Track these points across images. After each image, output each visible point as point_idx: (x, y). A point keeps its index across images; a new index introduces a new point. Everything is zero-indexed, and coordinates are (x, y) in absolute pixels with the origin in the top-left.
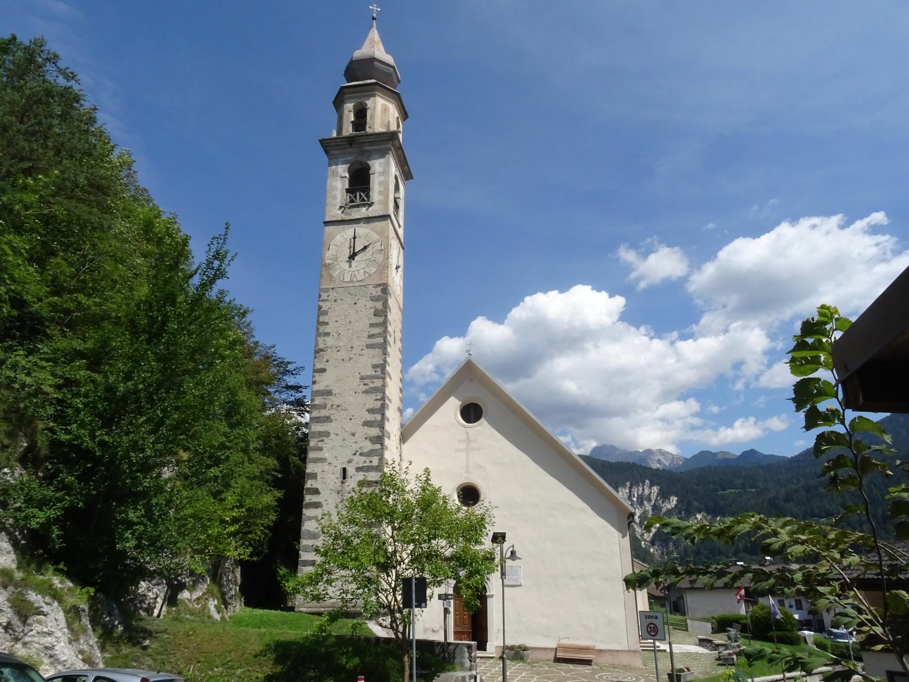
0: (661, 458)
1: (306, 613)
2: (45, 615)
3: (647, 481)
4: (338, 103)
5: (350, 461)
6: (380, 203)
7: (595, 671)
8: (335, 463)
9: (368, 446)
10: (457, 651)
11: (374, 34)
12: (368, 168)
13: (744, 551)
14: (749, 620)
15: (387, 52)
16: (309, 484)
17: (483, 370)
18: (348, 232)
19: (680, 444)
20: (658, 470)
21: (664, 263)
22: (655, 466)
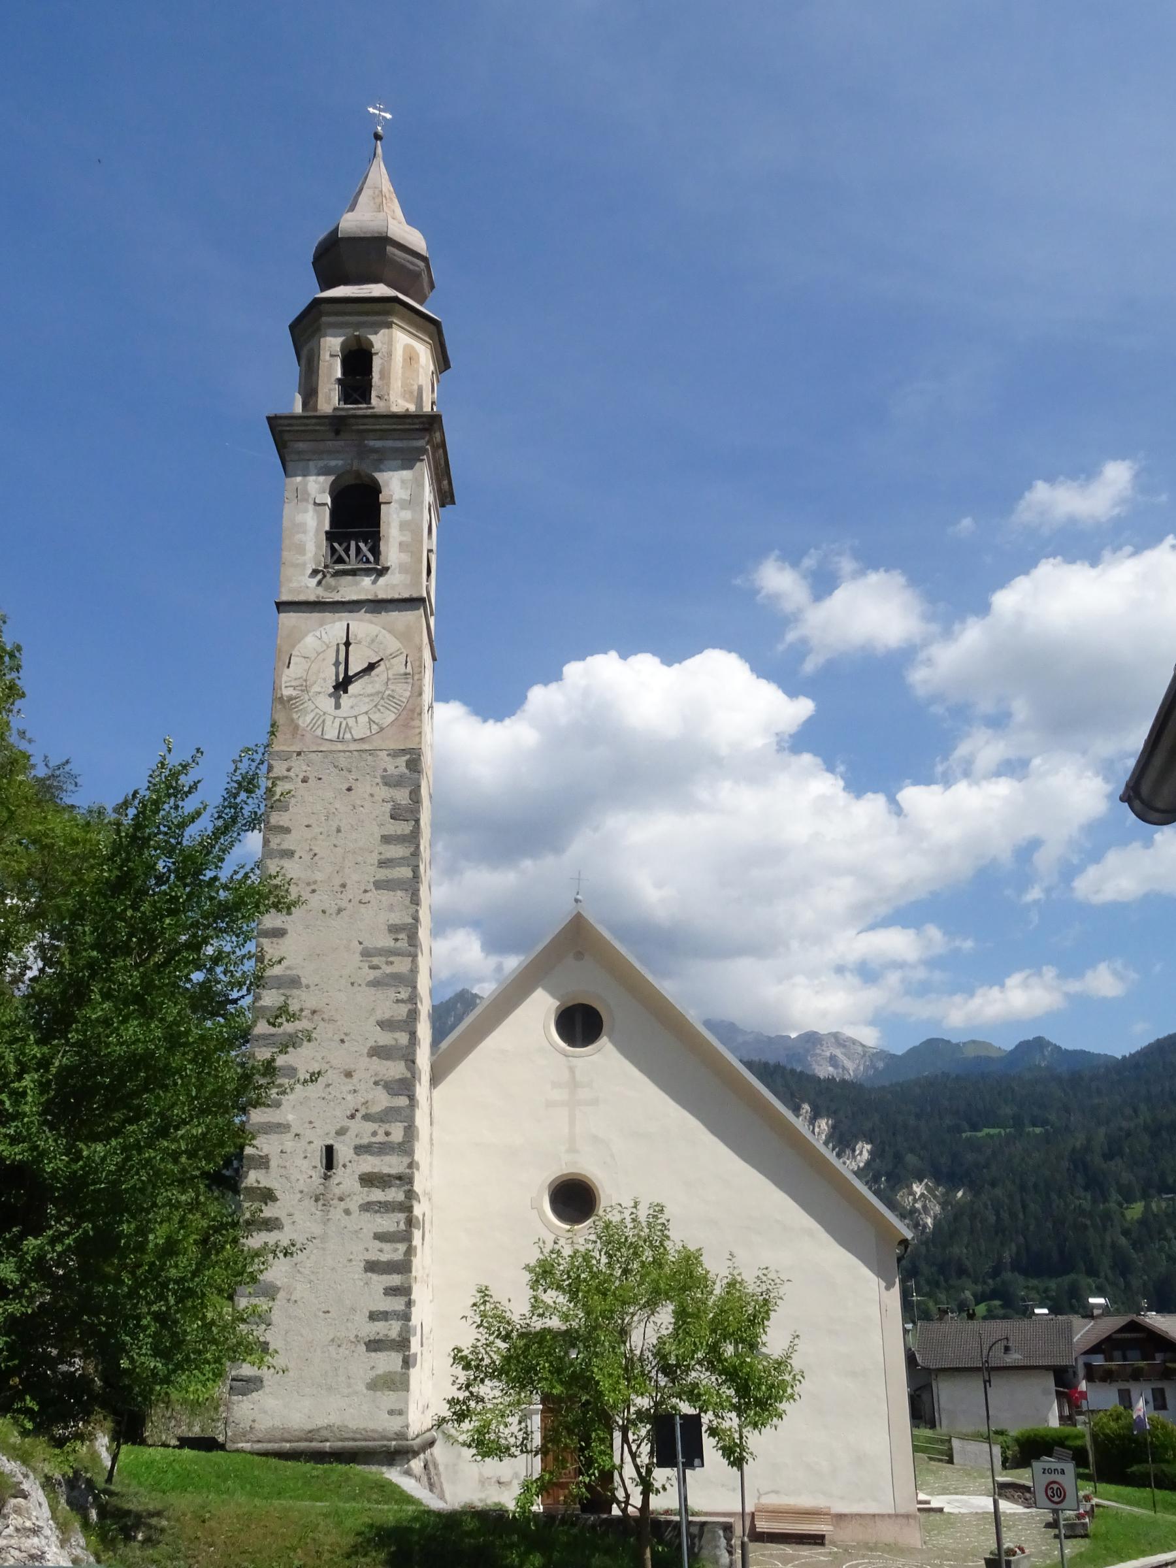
0: (838, 1052)
1: (252, 1453)
2: (25, 1497)
3: (806, 1107)
4: (306, 328)
5: (341, 1132)
6: (404, 569)
7: (837, 1560)
8: (308, 1134)
9: (382, 1100)
10: (707, 1536)
11: (379, 176)
12: (374, 490)
13: (1013, 1269)
14: (1088, 1438)
15: (410, 222)
16: (253, 1178)
17: (592, 921)
18: (334, 628)
19: (876, 1020)
20: (831, 1080)
21: (871, 611)
22: (824, 1071)
